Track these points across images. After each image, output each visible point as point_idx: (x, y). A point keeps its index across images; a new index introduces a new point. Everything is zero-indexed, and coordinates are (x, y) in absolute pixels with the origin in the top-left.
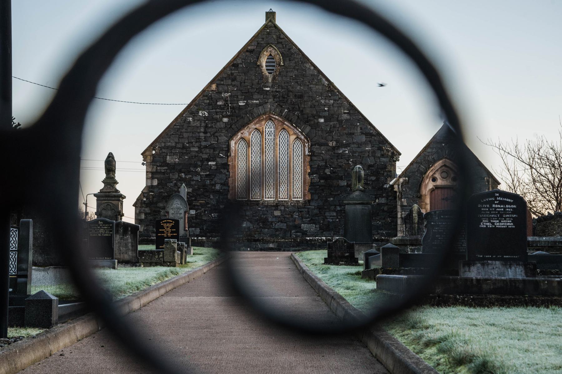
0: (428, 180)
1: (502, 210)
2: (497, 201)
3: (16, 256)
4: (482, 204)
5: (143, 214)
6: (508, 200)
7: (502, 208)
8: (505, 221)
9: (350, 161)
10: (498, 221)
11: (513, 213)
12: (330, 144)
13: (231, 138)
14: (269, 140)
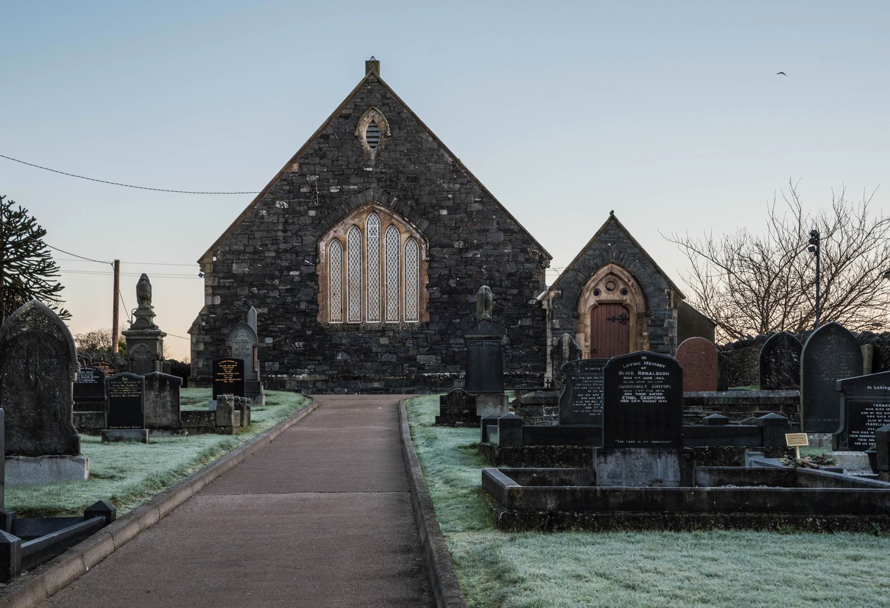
0: (588, 293)
4: (624, 370)
5: (202, 344)
6: (658, 365)
7: (650, 376)
8: (654, 394)
9: (483, 268)
10: (644, 394)
11: (665, 383)
12: (456, 245)
13: (320, 238)
14: (372, 240)
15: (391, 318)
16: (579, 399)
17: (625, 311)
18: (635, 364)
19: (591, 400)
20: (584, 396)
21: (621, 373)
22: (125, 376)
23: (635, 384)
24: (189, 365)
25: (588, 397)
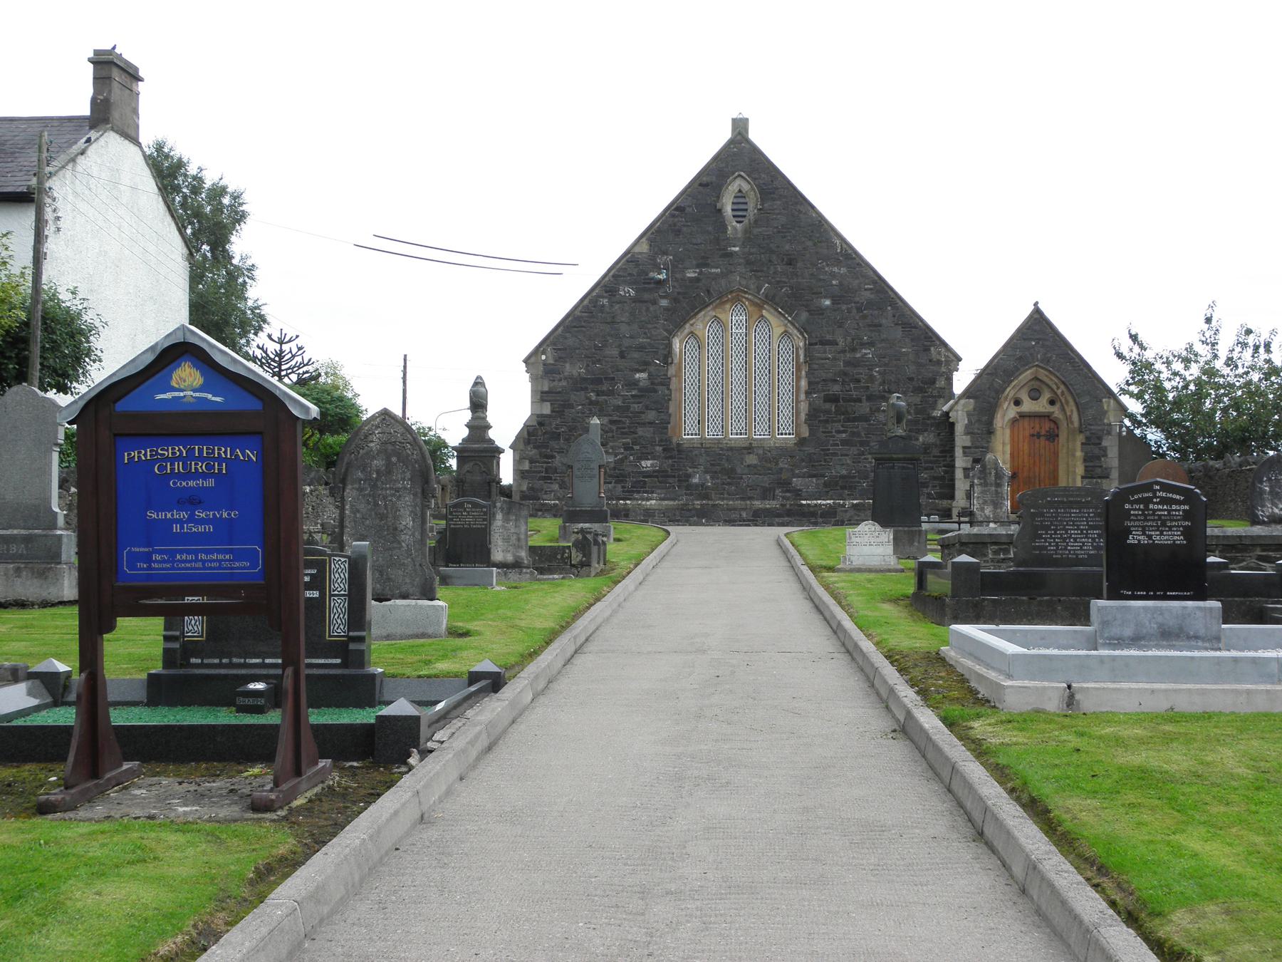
0: (1007, 403)
1: (1166, 513)
2: (1157, 497)
3: (346, 605)
4: (1132, 503)
5: (527, 461)
6: (1174, 496)
7: (1165, 510)
8: (1170, 533)
10: (1158, 533)
13: (672, 334)
15: (760, 434)
16: (1040, 537)
17: (1053, 425)
18: (1146, 495)
19: (1054, 539)
20: (1047, 534)
21: (1127, 506)
22: (468, 503)
23: (1146, 520)
24: (510, 486)
25: (1051, 534)
